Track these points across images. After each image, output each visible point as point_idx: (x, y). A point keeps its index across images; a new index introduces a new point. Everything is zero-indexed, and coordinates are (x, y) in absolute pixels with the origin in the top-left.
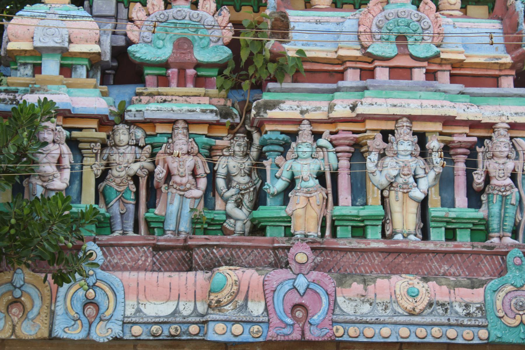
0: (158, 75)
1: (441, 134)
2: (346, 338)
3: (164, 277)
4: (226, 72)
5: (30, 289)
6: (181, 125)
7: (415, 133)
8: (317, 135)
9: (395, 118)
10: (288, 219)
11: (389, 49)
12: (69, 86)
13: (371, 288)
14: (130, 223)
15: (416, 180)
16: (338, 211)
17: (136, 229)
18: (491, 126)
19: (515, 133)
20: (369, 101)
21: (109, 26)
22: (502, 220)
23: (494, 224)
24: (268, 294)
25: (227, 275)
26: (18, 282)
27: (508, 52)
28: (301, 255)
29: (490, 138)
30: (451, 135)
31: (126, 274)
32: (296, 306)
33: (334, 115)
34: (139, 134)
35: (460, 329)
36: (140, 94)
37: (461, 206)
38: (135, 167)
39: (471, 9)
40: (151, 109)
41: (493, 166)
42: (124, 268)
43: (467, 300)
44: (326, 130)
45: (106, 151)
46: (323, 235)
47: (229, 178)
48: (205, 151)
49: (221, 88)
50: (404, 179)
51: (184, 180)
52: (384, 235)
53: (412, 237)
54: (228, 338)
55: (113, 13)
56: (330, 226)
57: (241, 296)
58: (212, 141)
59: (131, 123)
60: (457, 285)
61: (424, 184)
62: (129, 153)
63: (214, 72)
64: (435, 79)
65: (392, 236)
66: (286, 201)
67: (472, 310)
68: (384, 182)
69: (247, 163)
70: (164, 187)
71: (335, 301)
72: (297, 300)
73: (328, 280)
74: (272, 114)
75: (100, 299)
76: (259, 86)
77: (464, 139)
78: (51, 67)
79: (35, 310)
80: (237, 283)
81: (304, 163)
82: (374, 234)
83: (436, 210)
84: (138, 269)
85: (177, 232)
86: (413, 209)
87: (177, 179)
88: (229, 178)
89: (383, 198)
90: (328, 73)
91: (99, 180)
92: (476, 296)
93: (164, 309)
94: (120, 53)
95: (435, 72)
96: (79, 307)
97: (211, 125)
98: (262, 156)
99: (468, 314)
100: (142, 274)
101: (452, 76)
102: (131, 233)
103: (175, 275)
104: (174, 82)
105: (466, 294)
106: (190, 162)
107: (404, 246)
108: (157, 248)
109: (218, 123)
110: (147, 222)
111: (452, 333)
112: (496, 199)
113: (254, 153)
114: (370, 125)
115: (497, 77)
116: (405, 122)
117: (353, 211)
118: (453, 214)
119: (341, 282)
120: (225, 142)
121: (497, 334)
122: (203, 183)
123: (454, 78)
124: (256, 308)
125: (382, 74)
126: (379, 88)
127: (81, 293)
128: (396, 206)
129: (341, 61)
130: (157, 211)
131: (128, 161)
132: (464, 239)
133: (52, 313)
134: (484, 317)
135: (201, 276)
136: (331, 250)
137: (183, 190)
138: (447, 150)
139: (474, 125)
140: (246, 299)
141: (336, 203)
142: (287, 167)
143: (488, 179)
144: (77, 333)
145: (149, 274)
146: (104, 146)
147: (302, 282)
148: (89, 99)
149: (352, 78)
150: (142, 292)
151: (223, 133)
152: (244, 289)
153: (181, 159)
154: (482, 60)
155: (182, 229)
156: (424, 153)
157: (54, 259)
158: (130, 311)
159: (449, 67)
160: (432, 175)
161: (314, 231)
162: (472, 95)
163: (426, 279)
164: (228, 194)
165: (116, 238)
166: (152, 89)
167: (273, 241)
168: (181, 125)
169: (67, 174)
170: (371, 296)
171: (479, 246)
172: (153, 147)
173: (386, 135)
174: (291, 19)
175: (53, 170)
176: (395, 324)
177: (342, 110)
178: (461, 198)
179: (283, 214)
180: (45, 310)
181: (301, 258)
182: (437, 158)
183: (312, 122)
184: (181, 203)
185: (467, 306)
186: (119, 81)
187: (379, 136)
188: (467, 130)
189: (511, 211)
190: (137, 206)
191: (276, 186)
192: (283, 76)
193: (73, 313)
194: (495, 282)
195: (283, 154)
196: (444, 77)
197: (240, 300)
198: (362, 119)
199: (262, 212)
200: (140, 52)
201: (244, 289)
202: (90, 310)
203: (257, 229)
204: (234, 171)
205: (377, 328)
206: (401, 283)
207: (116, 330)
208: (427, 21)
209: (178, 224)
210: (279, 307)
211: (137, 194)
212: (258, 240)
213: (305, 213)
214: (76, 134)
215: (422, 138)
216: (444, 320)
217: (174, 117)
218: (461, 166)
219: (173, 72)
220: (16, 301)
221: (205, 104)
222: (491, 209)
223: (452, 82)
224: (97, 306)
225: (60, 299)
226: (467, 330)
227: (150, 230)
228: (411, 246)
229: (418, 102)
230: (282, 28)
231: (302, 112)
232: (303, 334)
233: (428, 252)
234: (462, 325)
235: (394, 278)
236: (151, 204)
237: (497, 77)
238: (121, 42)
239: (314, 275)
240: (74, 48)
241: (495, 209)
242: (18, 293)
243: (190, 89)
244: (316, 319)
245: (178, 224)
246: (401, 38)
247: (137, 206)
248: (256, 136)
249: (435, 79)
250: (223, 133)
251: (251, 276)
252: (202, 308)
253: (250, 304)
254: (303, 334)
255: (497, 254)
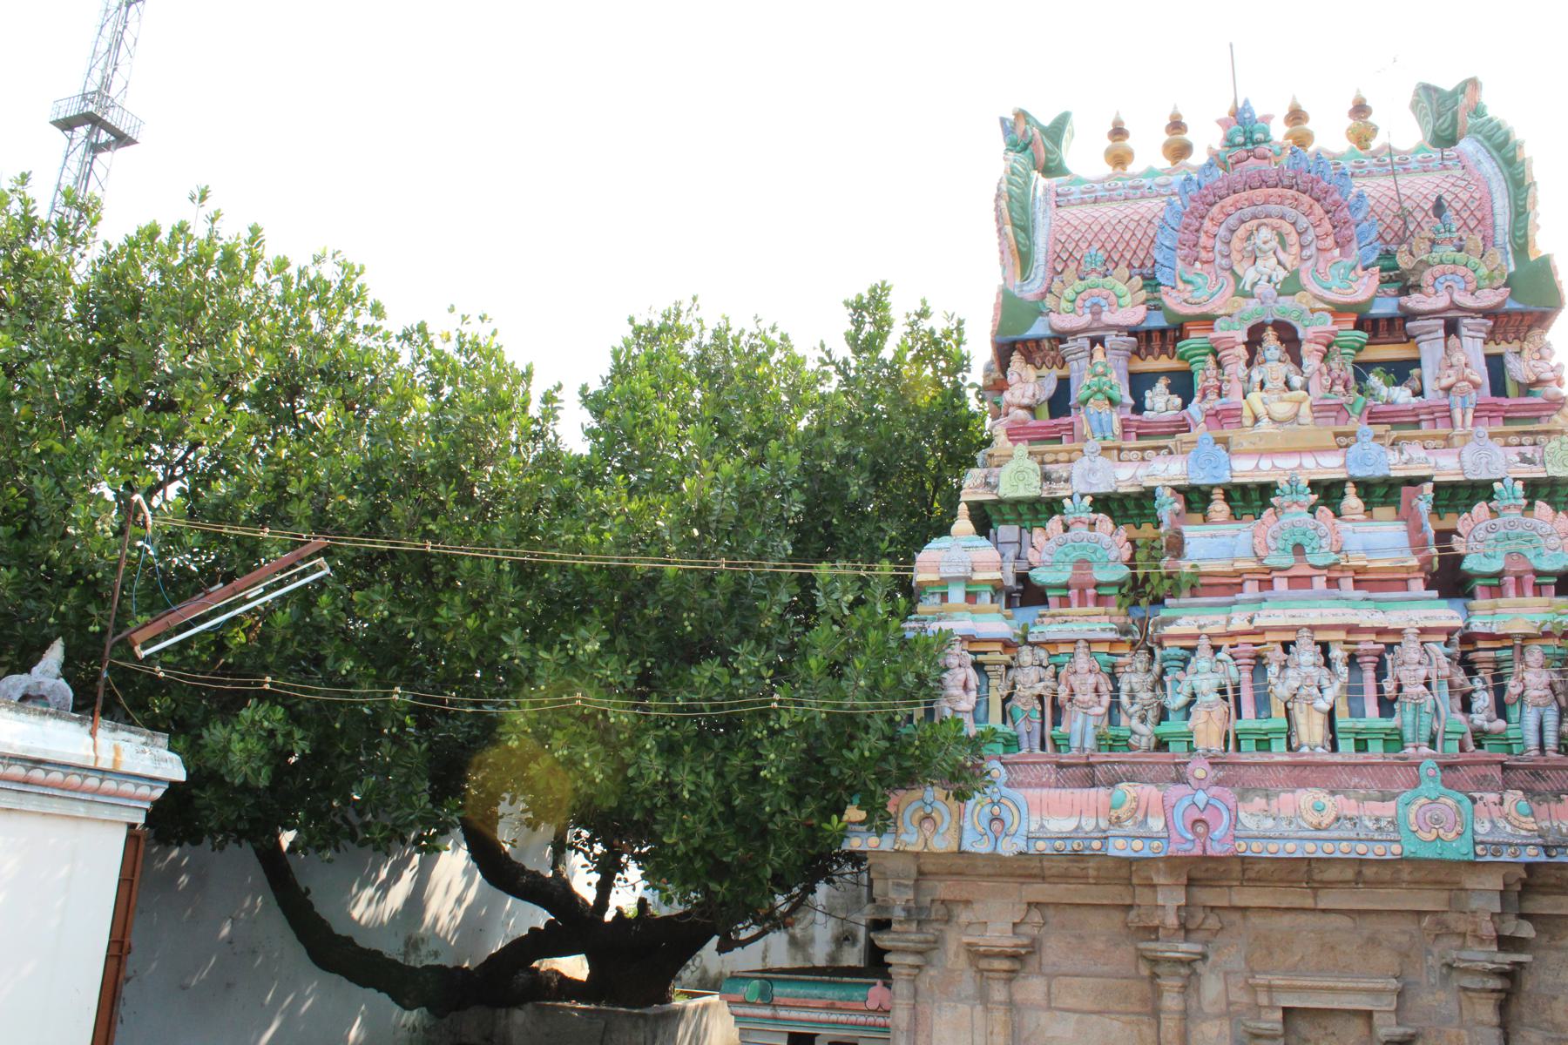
0: (1060, 597)
1: (1346, 642)
2: (1248, 854)
3: (1067, 793)
4: (1124, 591)
5: (939, 805)
6: (1082, 644)
7: (1317, 643)
8: (1216, 649)
9: (1296, 629)
10: (1190, 734)
11: (1288, 560)
12: (973, 612)
13: (1274, 802)
14: (1037, 741)
15: (1321, 691)
16: (1241, 725)
17: (1043, 747)
18: (1399, 632)
19: (1426, 638)
20: (1266, 613)
21: (1011, 552)
22: (1416, 730)
23: (1408, 734)
24: (1167, 810)
25: (1127, 791)
26: (929, 799)
27: (1415, 553)
28: (1199, 770)
29: (1399, 644)
30: (1356, 643)
31: (1030, 791)
32: (1196, 821)
33: (1232, 628)
34: (1042, 654)
35: (1370, 844)
36: (1042, 616)
37: (1371, 716)
38: (1039, 688)
39: (1377, 511)
40: (1052, 630)
41: (1403, 674)
42: (1029, 785)
43: (1377, 813)
44: (1225, 643)
45: (1011, 673)
46: (1226, 750)
47: (1132, 696)
48: (1108, 670)
49: (1120, 606)
50: (1309, 690)
51: (1087, 698)
52: (1290, 748)
53: (1319, 750)
54: (1128, 853)
55: (1016, 538)
56: (1233, 740)
57: (1141, 812)
58: (1114, 659)
59: (1033, 645)
60: (1367, 798)
61: (1329, 694)
62: (1033, 673)
63: (1115, 590)
64: (1338, 586)
65: (1298, 749)
66: (1188, 716)
67: (1383, 824)
68: (1287, 695)
69: (1150, 678)
70: (1068, 705)
71: (1237, 817)
72: (1197, 816)
73: (1229, 794)
74: (1169, 630)
75: (1005, 815)
76: (1158, 601)
77: (1371, 646)
78: (957, 595)
79: (945, 825)
80: (1137, 799)
81: (1204, 676)
82: (1279, 746)
83: (1342, 721)
84: (1042, 786)
85: (1082, 749)
86: (1319, 723)
87: (1079, 697)
88: (1132, 696)
89: (1287, 710)
90: (1227, 586)
91: (1005, 701)
92: (1388, 809)
93: (1066, 825)
94: (1023, 578)
95: (1337, 579)
96: (986, 824)
97: (1112, 642)
98: (1164, 672)
99: (1379, 828)
100: (1045, 791)
101: (1355, 581)
102: (1037, 751)
103: (1078, 791)
104: (1075, 602)
105: (1375, 808)
106: (1092, 679)
107: (1310, 759)
108: (1060, 766)
109: (1119, 641)
110: (1053, 740)
111: (1361, 848)
112: (1409, 708)
113: (1156, 668)
114: (1269, 637)
115: (1406, 581)
116: (1305, 633)
117: (1256, 724)
118: (1361, 724)
119: (1242, 797)
120: (1127, 659)
121: (1411, 849)
122: (1106, 700)
123: (1358, 584)
124: (1156, 824)
125: (1281, 585)
126: (1280, 598)
127: (987, 809)
128: (1300, 718)
129: (1239, 574)
130: (1061, 729)
131: (1031, 680)
132: (1376, 748)
133: (961, 829)
134: (1397, 831)
135: (1102, 791)
136: (1234, 764)
137: (1086, 707)
138: (1352, 660)
139: (1381, 632)
140: (1146, 815)
141: (1239, 716)
142: (1189, 681)
143: (1399, 688)
144: (984, 848)
145: (1052, 791)
146: (1009, 667)
147: (1201, 797)
148: (994, 623)
149: (1251, 590)
150: (1045, 808)
151: (1125, 649)
152: (1143, 805)
153: (1084, 677)
154: (1386, 564)
155: (1087, 745)
156: (1328, 663)
157: (954, 778)
158: (1034, 827)
159: (1351, 574)
160: (1337, 685)
161: (1216, 746)
162: (1376, 600)
163: (1333, 793)
164: (1132, 710)
165: (1024, 756)
166: (1053, 611)
167: (1174, 757)
168: (1082, 644)
169: (973, 695)
170: (1274, 810)
171: (1391, 758)
172: (1057, 666)
173: (1286, 646)
174: (1186, 535)
175: (959, 695)
176: (1300, 839)
177: (1239, 623)
178: (1371, 708)
179: (1185, 729)
180: (954, 825)
181: (1200, 773)
182: (1342, 668)
183: (1210, 636)
184: (1085, 721)
185: (1377, 820)
186: (1025, 603)
187: (1279, 648)
188: (1373, 637)
189: (1426, 719)
190: (1043, 724)
191: (1176, 701)
192: (1180, 591)
193: (980, 829)
194: (1408, 795)
195: (1184, 669)
196: (1347, 584)
197: (1140, 817)
198: (1261, 631)
199: (1165, 728)
200: (1040, 576)
201: (1143, 805)
202: (996, 825)
203: (1161, 745)
204: (1136, 687)
205: (1281, 843)
206: (1306, 798)
207: (1021, 845)
208: (1324, 529)
209: (1083, 741)
210: (1179, 822)
211: (1042, 713)
212: (1161, 756)
213: (1208, 727)
214: (981, 658)
215: (1325, 647)
216: (1353, 835)
217: (1075, 637)
218: (1369, 675)
219: (1073, 593)
220: (927, 817)
221: (1105, 622)
222: (1404, 718)
223: (1356, 588)
224: (1002, 821)
225: (968, 814)
226: (1378, 845)
227: (1057, 747)
228: (1318, 759)
229: (1317, 612)
230: (1177, 546)
231: (1200, 627)
232: (1204, 850)
233: (1336, 764)
234: (1372, 840)
235: (1299, 792)
236: (1056, 722)
237: (1406, 581)
238: (1023, 566)
239: (1215, 790)
240: (978, 576)
241: (1409, 718)
242: (928, 809)
243: (1091, 608)
244: (1217, 834)
245: (1083, 741)
246: (1298, 549)
247: (1043, 724)
248: (1157, 651)
249: (1338, 586)
250: (1125, 649)
251: (1150, 792)
252: (1103, 824)
253: (1150, 820)
254: (1204, 850)
255: (1411, 765)
